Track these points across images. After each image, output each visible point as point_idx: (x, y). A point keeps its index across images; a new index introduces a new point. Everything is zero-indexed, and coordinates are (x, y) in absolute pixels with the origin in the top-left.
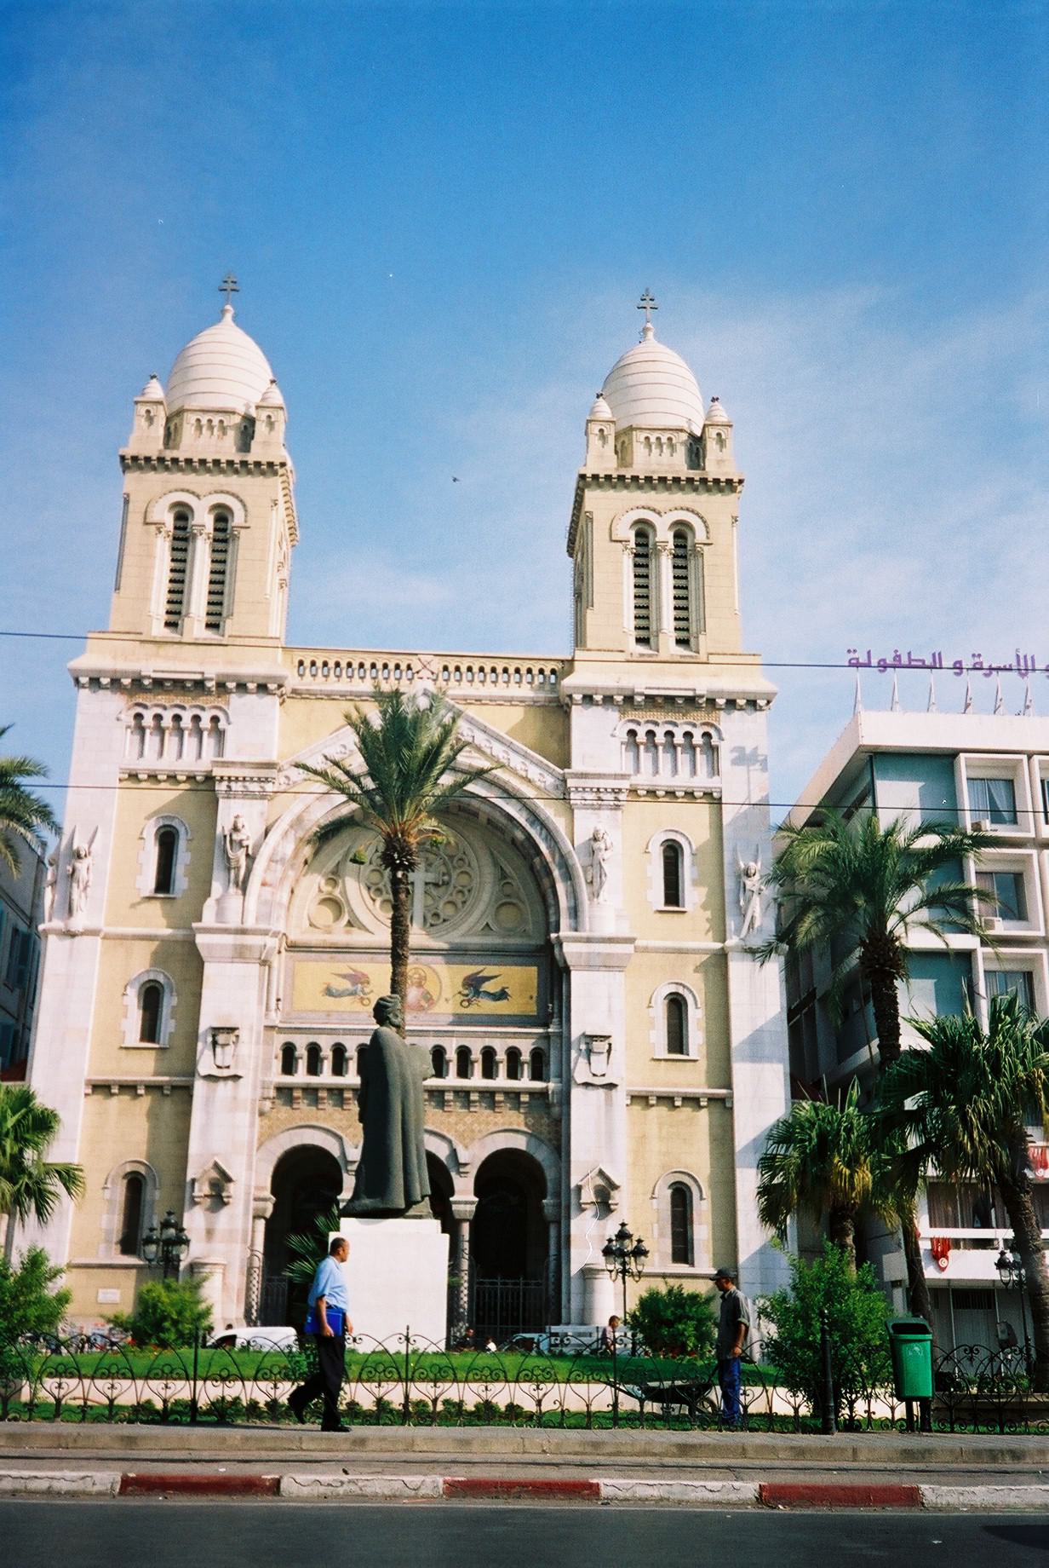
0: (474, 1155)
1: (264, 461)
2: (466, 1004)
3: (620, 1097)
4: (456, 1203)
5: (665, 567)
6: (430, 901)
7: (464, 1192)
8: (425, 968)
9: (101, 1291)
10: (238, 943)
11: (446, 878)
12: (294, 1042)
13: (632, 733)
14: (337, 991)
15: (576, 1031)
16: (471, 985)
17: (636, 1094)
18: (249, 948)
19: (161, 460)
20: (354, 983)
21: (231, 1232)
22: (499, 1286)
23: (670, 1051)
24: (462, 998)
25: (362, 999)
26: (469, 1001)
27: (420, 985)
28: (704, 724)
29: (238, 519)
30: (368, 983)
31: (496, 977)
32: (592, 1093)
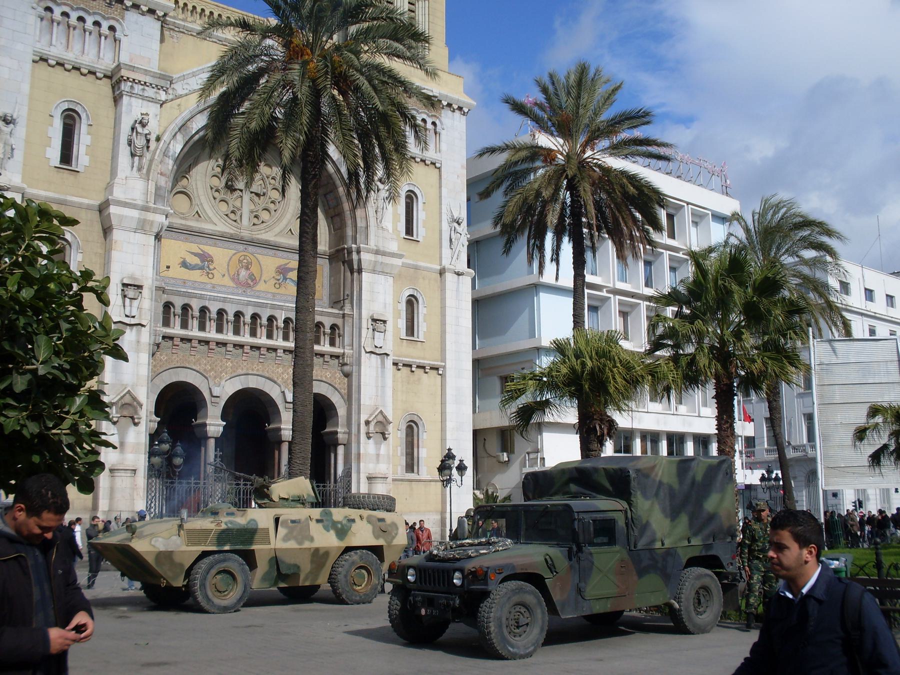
0: (228, 388)
2: (277, 286)
3: (389, 362)
4: (210, 425)
6: (253, 207)
7: (214, 417)
8: (252, 257)
10: (142, 217)
11: (265, 190)
13: (48, 9)
15: (365, 314)
16: (280, 273)
17: (406, 363)
20: (203, 261)
22: (193, 485)
23: (407, 335)
25: (208, 273)
26: (279, 284)
27: (247, 268)
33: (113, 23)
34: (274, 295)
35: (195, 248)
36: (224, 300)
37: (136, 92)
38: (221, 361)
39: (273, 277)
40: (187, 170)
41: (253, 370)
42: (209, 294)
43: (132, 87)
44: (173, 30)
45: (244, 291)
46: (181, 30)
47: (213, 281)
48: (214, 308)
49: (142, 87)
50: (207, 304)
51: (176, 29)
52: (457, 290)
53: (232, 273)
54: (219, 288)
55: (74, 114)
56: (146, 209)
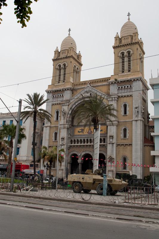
1: (71, 55)
5: (126, 59)
18: (65, 127)
19: (119, 46)
21: (64, 165)
29: (131, 53)
32: (110, 144)
35: (80, 128)
52: (136, 125)
56: (64, 125)
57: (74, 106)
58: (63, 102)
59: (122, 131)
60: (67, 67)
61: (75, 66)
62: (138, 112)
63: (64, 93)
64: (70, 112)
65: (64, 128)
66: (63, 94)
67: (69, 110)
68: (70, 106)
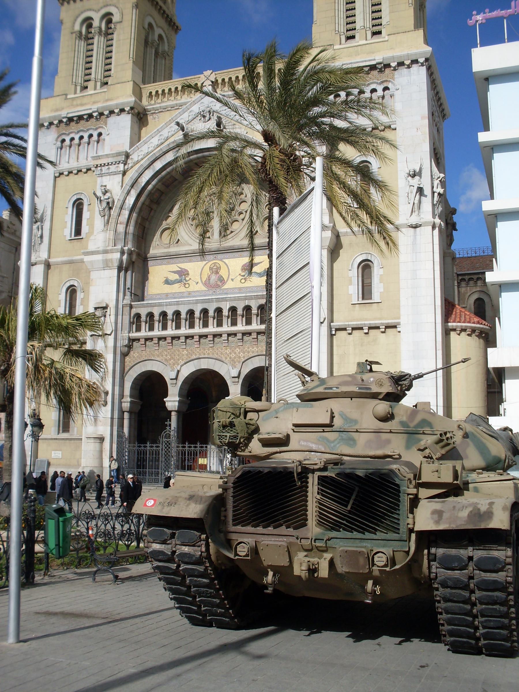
2: (243, 281)
4: (170, 401)
7: (174, 395)
9: (53, 452)
12: (165, 310)
14: (171, 281)
17: (338, 327)
20: (180, 276)
24: (241, 278)
25: (185, 284)
26: (245, 279)
28: (382, 82)
30: (188, 274)
31: (261, 262)
33: (100, 130)
34: (240, 289)
35: (175, 267)
36: (178, 303)
37: (103, 172)
38: (179, 351)
39: (240, 274)
40: (329, 193)
41: (204, 354)
42: (164, 301)
43: (101, 170)
44: (155, 113)
45: (214, 292)
46: (160, 110)
47: (188, 290)
48: (170, 312)
49: (107, 167)
50: (165, 309)
51: (157, 112)
53: (204, 280)
54: (193, 294)
55: (367, 164)
56: (106, 252)
57: (148, 175)
58: (99, 162)
59: (354, 274)
60: (118, 26)
61: (150, 25)
62: (420, 190)
63: (106, 124)
64: (131, 200)
65: (106, 265)
66: (100, 130)
67: (128, 193)
68: (131, 175)
